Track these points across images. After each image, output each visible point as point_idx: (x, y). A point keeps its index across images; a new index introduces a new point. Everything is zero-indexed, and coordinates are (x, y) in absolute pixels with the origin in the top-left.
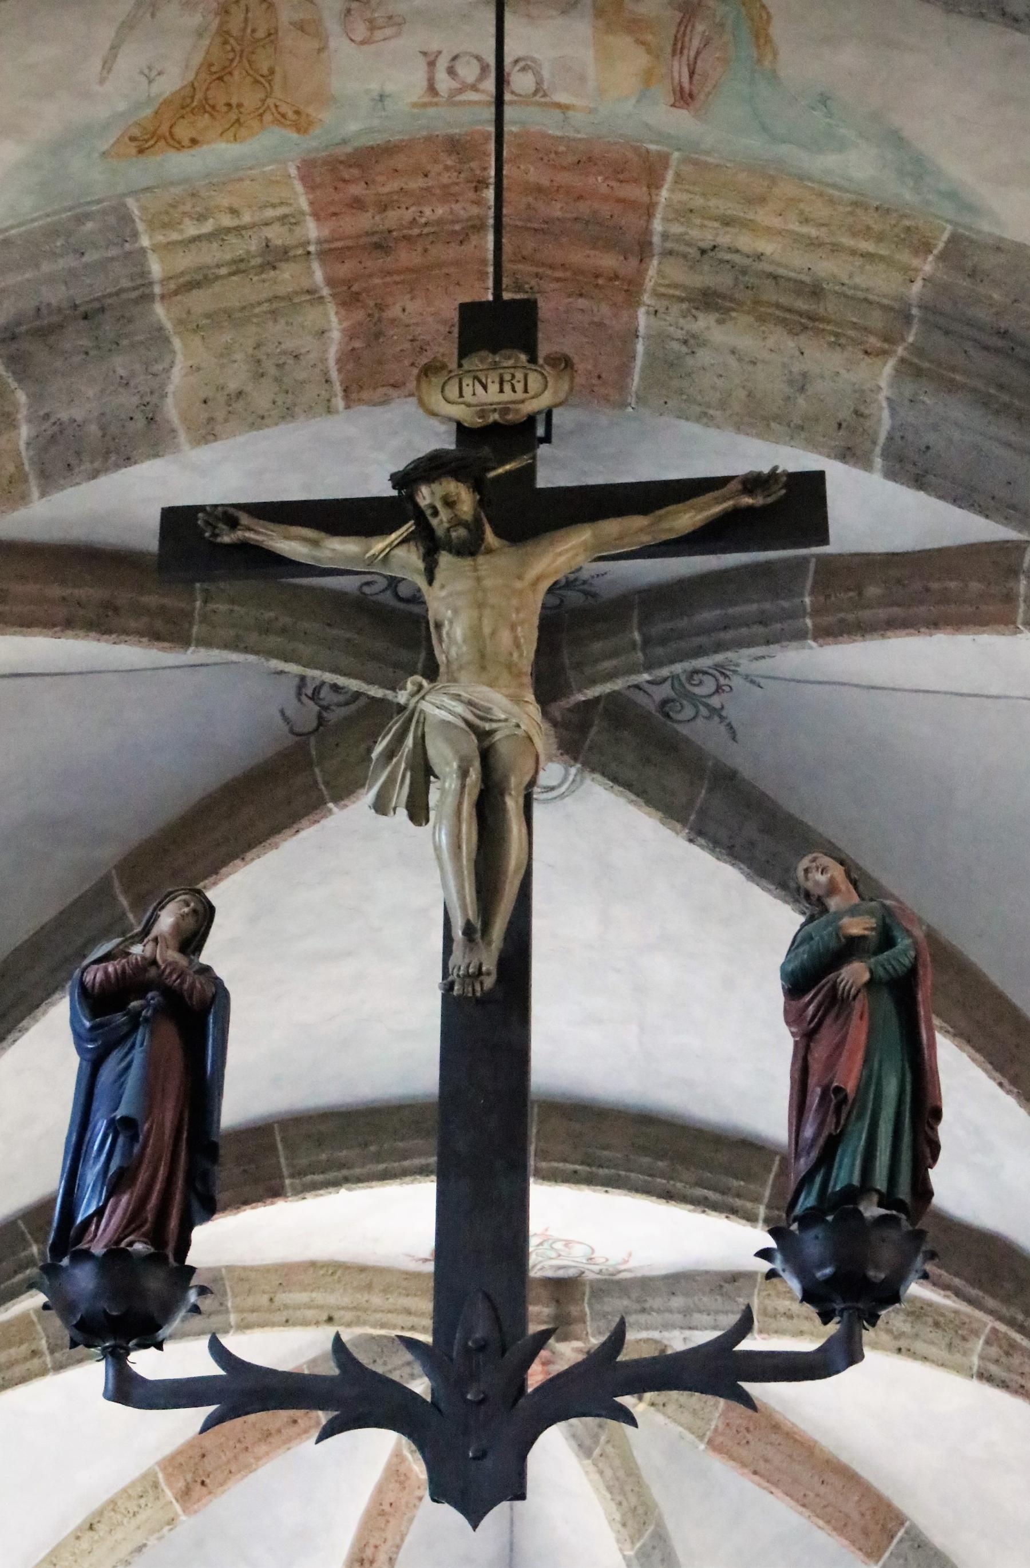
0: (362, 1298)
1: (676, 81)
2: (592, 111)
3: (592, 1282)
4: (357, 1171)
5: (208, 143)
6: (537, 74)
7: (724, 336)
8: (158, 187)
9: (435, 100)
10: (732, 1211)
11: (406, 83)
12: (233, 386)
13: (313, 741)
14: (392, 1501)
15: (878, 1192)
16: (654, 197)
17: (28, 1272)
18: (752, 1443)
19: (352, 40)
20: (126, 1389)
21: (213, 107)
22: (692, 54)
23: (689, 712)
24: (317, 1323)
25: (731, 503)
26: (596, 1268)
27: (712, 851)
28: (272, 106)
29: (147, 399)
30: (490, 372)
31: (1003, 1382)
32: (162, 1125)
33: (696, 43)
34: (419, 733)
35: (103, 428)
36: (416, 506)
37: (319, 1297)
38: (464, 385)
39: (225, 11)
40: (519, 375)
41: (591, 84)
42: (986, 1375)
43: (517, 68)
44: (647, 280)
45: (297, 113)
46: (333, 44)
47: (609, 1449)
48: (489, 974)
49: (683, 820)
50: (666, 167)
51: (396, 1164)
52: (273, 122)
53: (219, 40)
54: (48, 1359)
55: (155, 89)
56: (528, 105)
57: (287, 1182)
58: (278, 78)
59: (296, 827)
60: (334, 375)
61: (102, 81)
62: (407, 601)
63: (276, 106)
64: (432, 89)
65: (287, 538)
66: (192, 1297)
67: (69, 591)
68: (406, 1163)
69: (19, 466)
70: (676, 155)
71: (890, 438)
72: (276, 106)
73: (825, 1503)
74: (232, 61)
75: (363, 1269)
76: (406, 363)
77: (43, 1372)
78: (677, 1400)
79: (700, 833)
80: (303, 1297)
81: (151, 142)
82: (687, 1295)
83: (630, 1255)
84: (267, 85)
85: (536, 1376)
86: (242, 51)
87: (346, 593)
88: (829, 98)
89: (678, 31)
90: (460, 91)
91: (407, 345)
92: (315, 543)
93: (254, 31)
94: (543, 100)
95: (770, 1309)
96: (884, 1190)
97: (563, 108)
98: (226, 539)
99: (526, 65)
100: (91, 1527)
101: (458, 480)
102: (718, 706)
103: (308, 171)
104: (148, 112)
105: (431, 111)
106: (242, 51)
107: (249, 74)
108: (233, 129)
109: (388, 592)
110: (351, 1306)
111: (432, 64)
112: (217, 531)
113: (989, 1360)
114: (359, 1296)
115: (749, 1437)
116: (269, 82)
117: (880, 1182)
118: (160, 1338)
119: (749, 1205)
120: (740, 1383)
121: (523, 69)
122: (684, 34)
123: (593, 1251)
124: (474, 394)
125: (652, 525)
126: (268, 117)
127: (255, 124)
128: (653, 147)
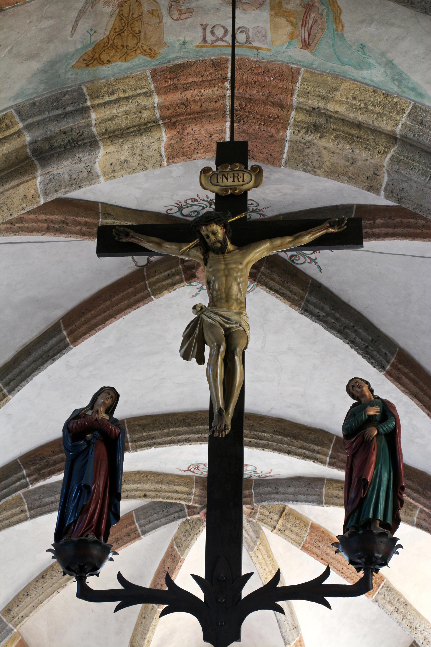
0: (159, 486)
1: (303, 38)
2: (269, 50)
3: (256, 480)
4: (159, 440)
5: (115, 62)
6: (247, 34)
7: (327, 145)
8: (93, 80)
9: (206, 44)
10: (315, 460)
11: (194, 37)
12: (122, 158)
13: (145, 269)
14: (169, 566)
15: (379, 520)
16: (294, 86)
17: (22, 481)
18: (321, 547)
19: (172, 19)
20: (85, 593)
21: (116, 47)
22: (310, 26)
23: (302, 260)
24: (140, 497)
25: (325, 231)
26: (257, 475)
27: (311, 319)
28: (140, 46)
29: (88, 164)
30: (229, 173)
31: (427, 528)
32: (99, 486)
33: (311, 22)
34: (201, 327)
35: (70, 176)
36: (201, 234)
37: (140, 486)
38: (219, 177)
39: (121, 5)
40: (241, 175)
41: (269, 38)
42: (420, 525)
43: (239, 31)
44: (291, 119)
45: (150, 49)
46: (164, 21)
47: (261, 547)
48: (228, 429)
49: (299, 305)
50: (299, 74)
51: (175, 438)
52: (140, 53)
53: (119, 18)
54: (28, 514)
55: (93, 39)
56: (243, 47)
57: (130, 444)
58: (143, 33)
59: (138, 305)
60: (163, 154)
61: (72, 36)
62: (186, 216)
63: (142, 47)
64: (204, 40)
65: (148, 242)
66: (110, 555)
67: (48, 217)
68: (180, 437)
69: (36, 191)
70: (303, 69)
71: (388, 184)
72: (142, 47)
73: (351, 572)
74: (124, 27)
75: (159, 474)
76: (193, 148)
77: (26, 519)
78: (290, 529)
79: (306, 310)
80: (134, 486)
81: (92, 62)
82: (295, 487)
83: (272, 470)
84: (138, 37)
85: (246, 592)
86: (128, 23)
87: (161, 213)
88: (364, 46)
89: (304, 17)
90: (216, 41)
91: (193, 142)
92: (159, 245)
93: (133, 14)
94: (249, 45)
95: (330, 494)
96: (382, 520)
97: (257, 49)
98: (124, 240)
99: (244, 30)
100: (43, 577)
101: (217, 224)
102: (314, 258)
103: (154, 73)
104: (90, 49)
105: (204, 49)
106: (128, 23)
107: (131, 33)
108: (124, 56)
109: (179, 212)
110: (154, 490)
111: (205, 29)
112: (120, 237)
113: (421, 519)
114: (157, 486)
115: (320, 544)
116: (139, 36)
117: (380, 516)
118: (98, 572)
119: (322, 457)
120: (324, 597)
121: (241, 32)
122: (306, 18)
123: (256, 469)
124: (223, 182)
125: (293, 241)
126: (138, 51)
127: (133, 54)
128: (293, 66)
